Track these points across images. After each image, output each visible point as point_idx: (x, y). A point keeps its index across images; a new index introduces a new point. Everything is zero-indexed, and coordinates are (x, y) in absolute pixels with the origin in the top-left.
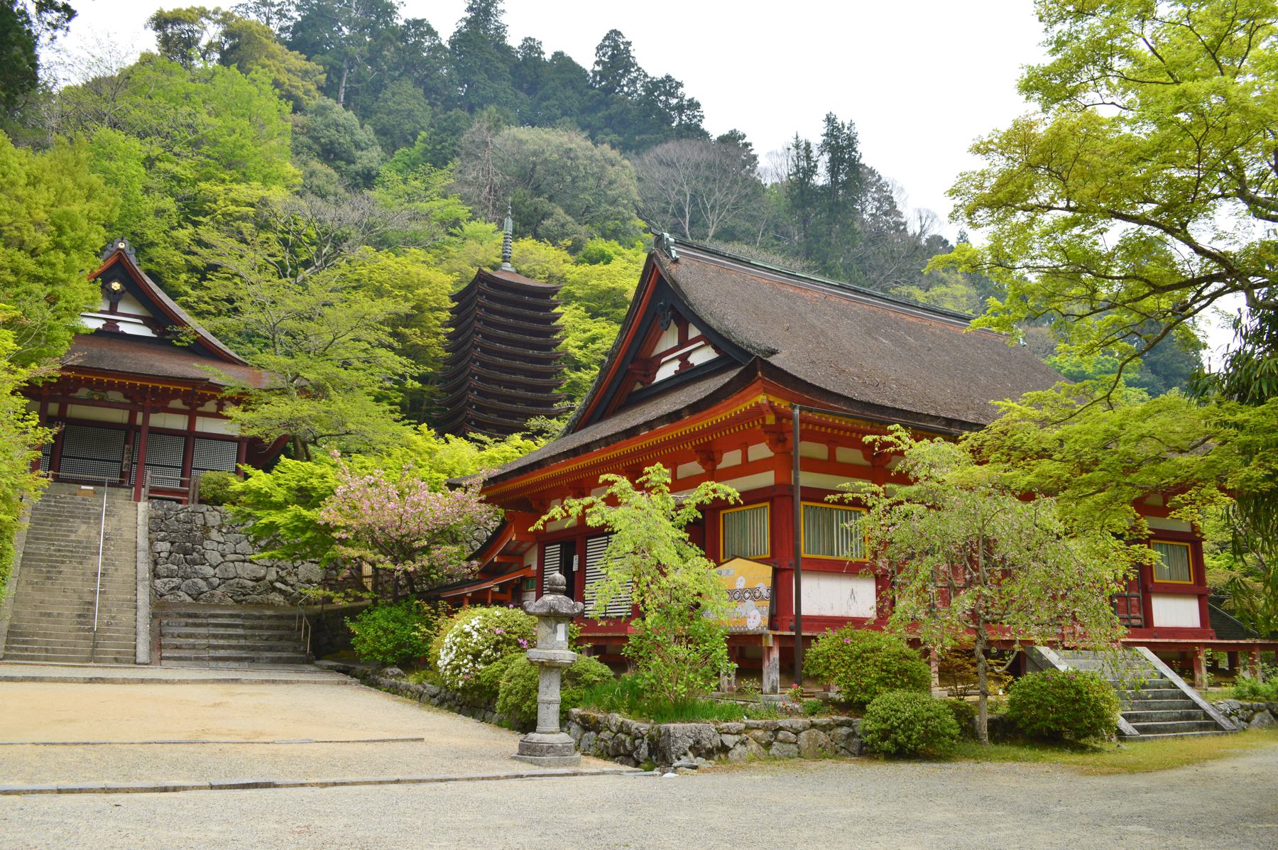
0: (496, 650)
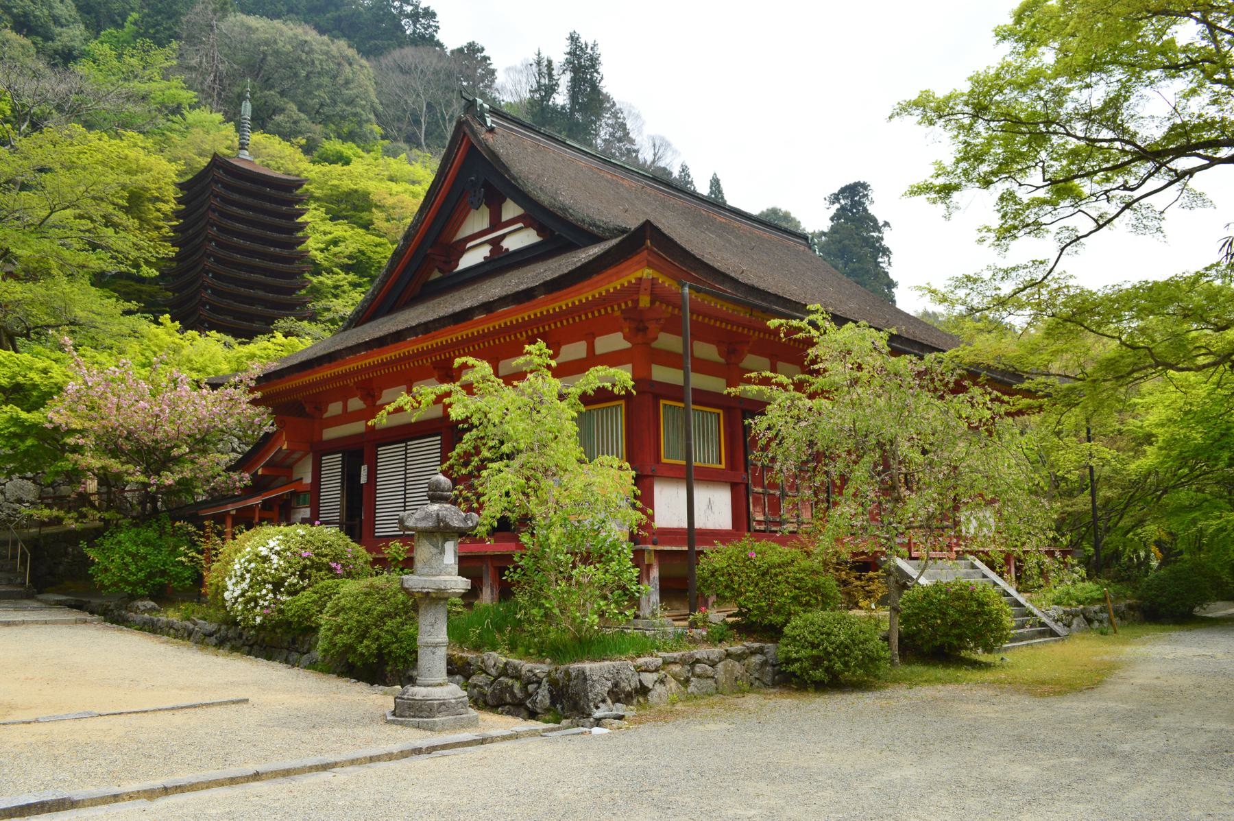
0: (302, 577)
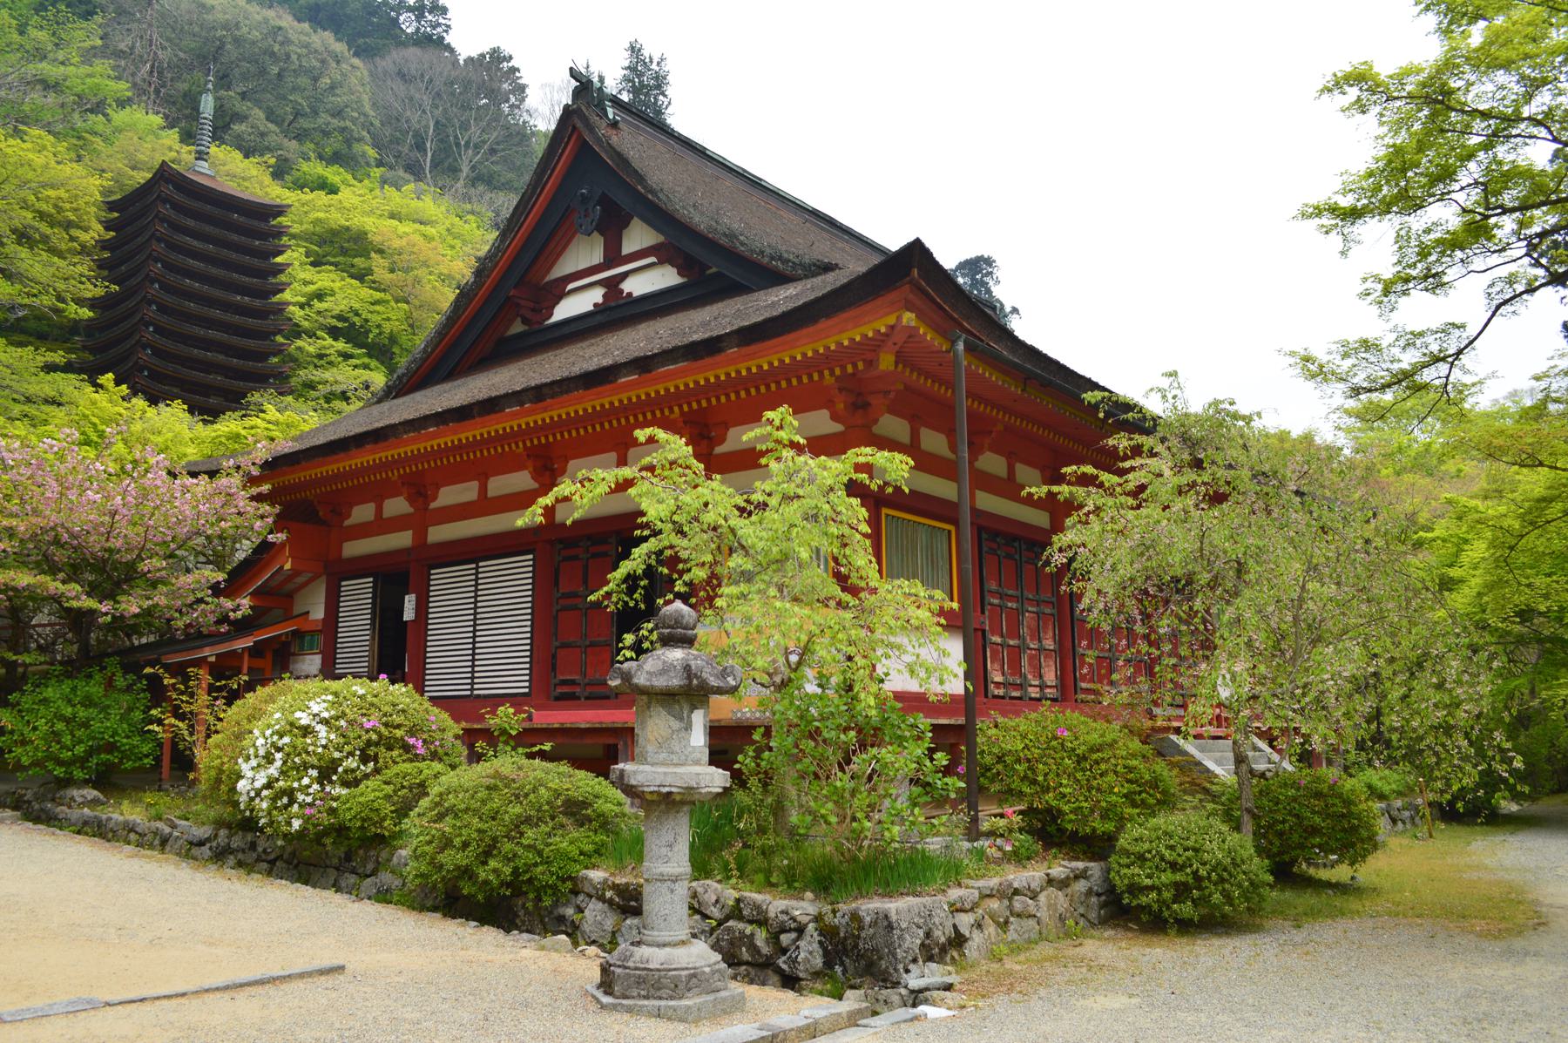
0: (365, 759)
